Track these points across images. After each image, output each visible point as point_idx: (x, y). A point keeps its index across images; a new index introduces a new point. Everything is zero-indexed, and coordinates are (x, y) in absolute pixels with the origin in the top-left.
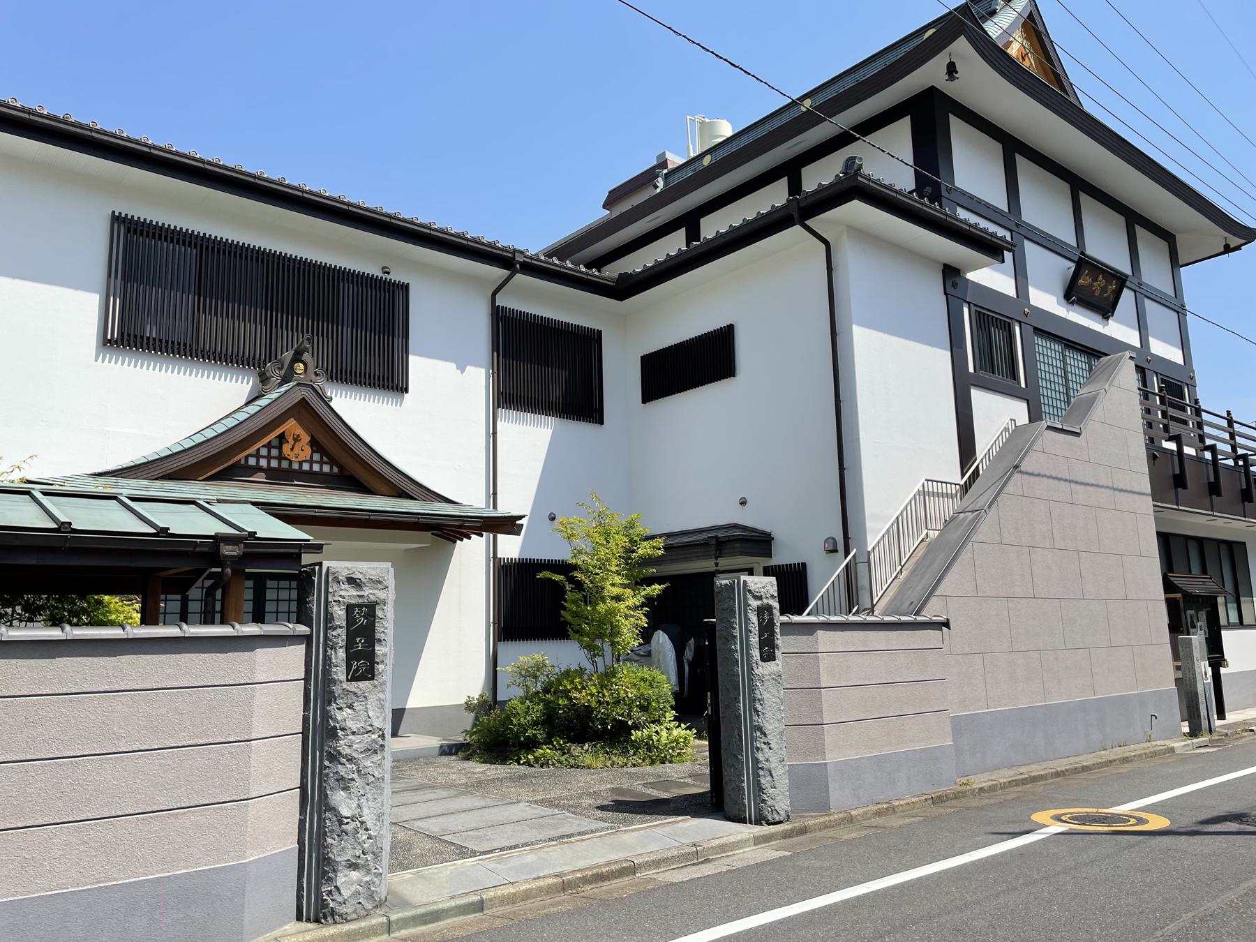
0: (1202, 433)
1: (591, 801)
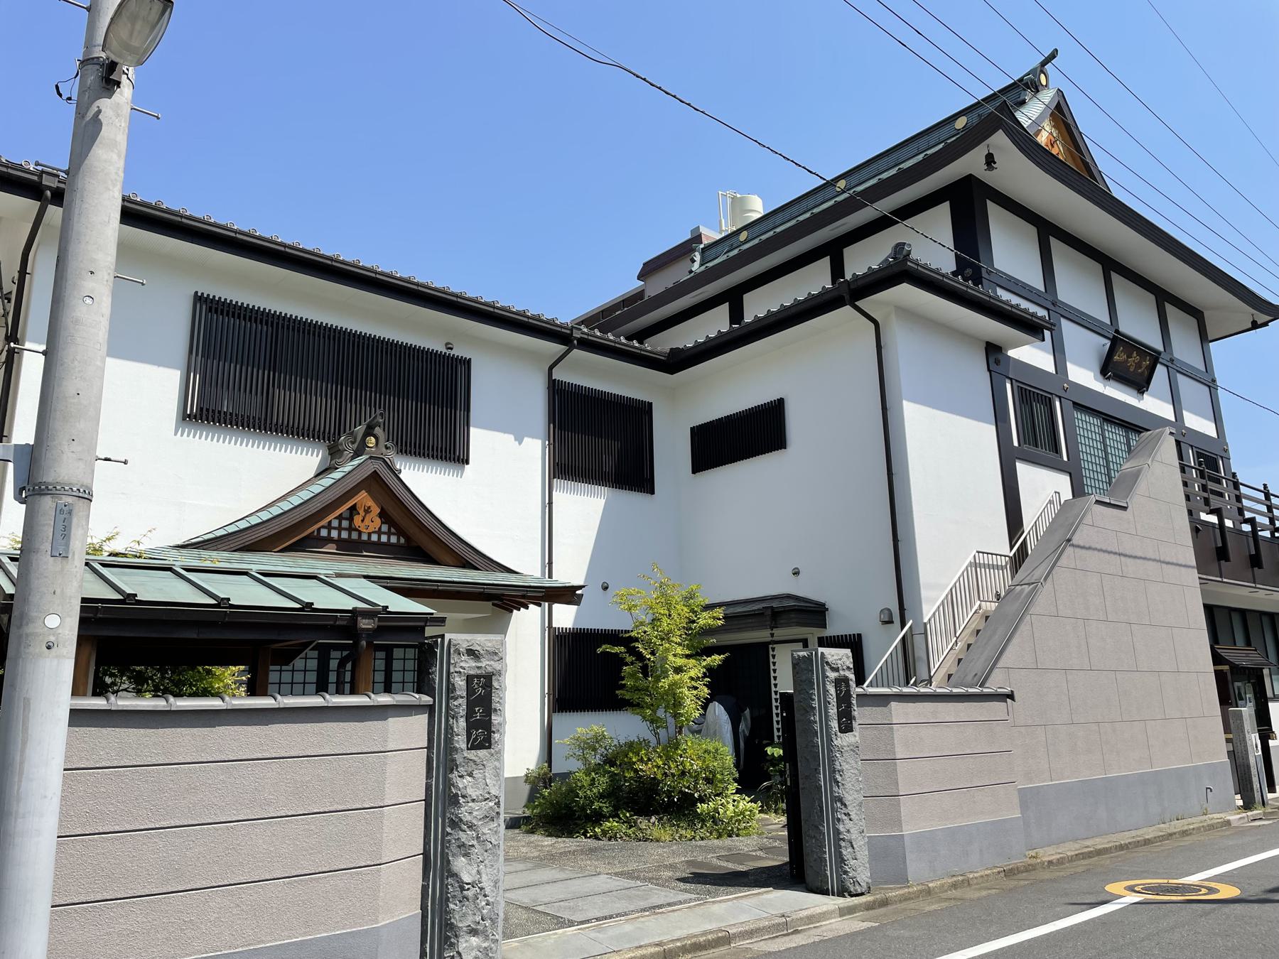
0: (1241, 506)
1: (670, 874)
